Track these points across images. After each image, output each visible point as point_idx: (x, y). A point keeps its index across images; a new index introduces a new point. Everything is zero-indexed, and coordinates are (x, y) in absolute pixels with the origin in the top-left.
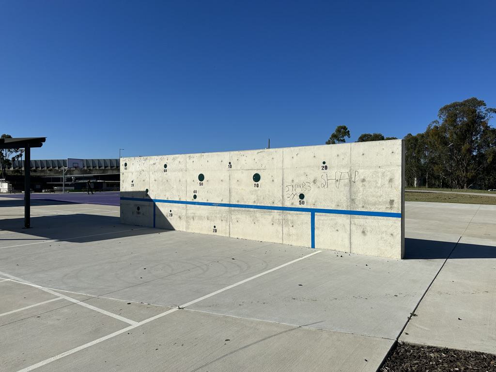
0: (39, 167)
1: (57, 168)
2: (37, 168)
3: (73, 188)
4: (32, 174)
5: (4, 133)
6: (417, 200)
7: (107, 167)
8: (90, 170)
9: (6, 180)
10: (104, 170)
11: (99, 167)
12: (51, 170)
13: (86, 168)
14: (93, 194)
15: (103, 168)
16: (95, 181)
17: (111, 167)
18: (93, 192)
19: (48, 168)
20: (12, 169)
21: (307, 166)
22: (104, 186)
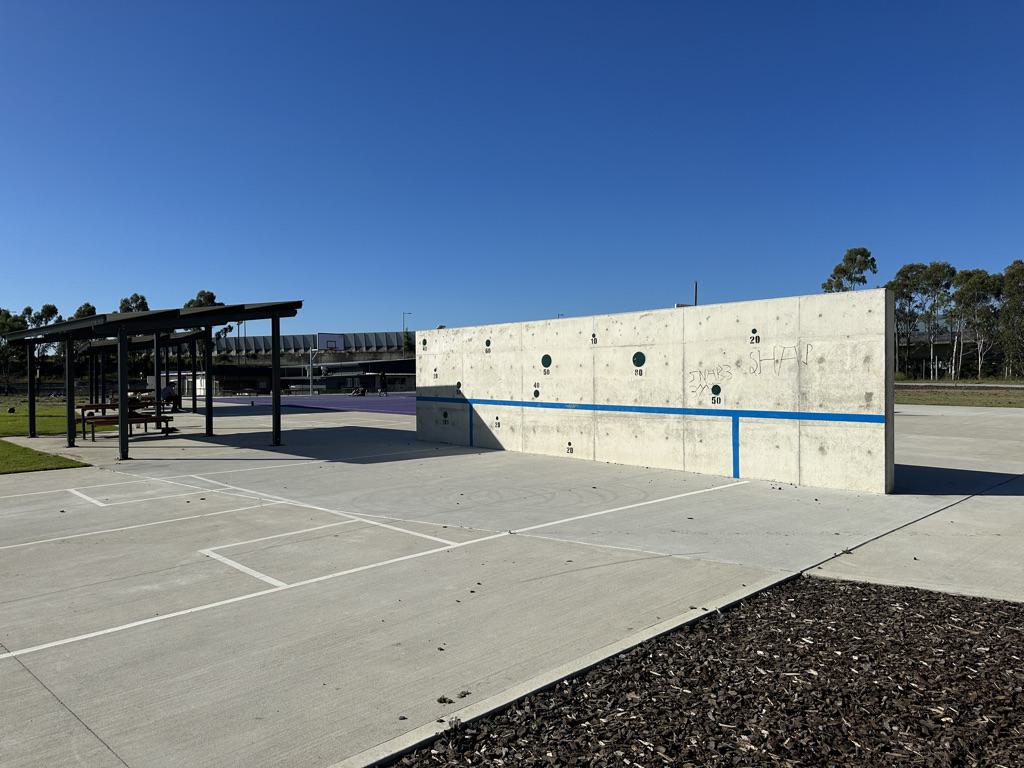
0: (261, 350)
2: (257, 351)
3: (324, 387)
8: (351, 353)
11: (367, 348)
15: (374, 349)
16: (361, 373)
17: (389, 347)
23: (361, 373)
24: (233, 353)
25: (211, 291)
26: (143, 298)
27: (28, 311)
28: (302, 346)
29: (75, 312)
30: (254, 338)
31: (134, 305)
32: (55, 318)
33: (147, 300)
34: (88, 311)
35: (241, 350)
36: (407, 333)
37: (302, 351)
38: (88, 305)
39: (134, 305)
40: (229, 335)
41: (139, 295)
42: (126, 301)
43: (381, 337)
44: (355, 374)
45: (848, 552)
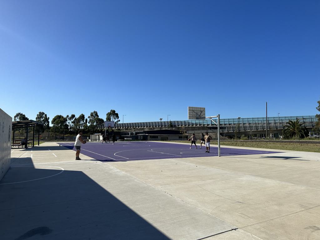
0: (129, 127)
1: (137, 127)
2: (128, 127)
3: (131, 139)
4: (28, 144)
5: (72, 114)
6: (302, 150)
7: (163, 126)
8: (154, 128)
9: (101, 134)
10: (161, 128)
11: (159, 126)
12: (134, 129)
13: (151, 127)
14: (78, 158)
15: (160, 127)
16: (144, 134)
17: (165, 126)
18: (81, 156)
19: (133, 127)
20: (117, 128)
21: (310, 227)
22: (149, 138)
23: (144, 134)
24: (122, 128)
25: (114, 110)
26: (97, 112)
27: (68, 116)
28: (180, 125)
29: (79, 116)
30: (135, 123)
31: (94, 114)
32: (75, 118)
33: (98, 113)
34: (23, 117)
35: (124, 127)
36: (170, 121)
37: (140, 127)
38: (82, 114)
39: (94, 114)
40: (119, 123)
41: (96, 111)
42: (92, 113)
43: (179, 122)
44: (143, 134)
45: (235, 229)
